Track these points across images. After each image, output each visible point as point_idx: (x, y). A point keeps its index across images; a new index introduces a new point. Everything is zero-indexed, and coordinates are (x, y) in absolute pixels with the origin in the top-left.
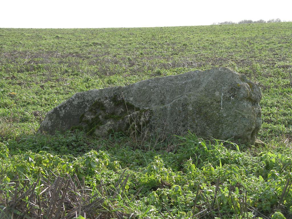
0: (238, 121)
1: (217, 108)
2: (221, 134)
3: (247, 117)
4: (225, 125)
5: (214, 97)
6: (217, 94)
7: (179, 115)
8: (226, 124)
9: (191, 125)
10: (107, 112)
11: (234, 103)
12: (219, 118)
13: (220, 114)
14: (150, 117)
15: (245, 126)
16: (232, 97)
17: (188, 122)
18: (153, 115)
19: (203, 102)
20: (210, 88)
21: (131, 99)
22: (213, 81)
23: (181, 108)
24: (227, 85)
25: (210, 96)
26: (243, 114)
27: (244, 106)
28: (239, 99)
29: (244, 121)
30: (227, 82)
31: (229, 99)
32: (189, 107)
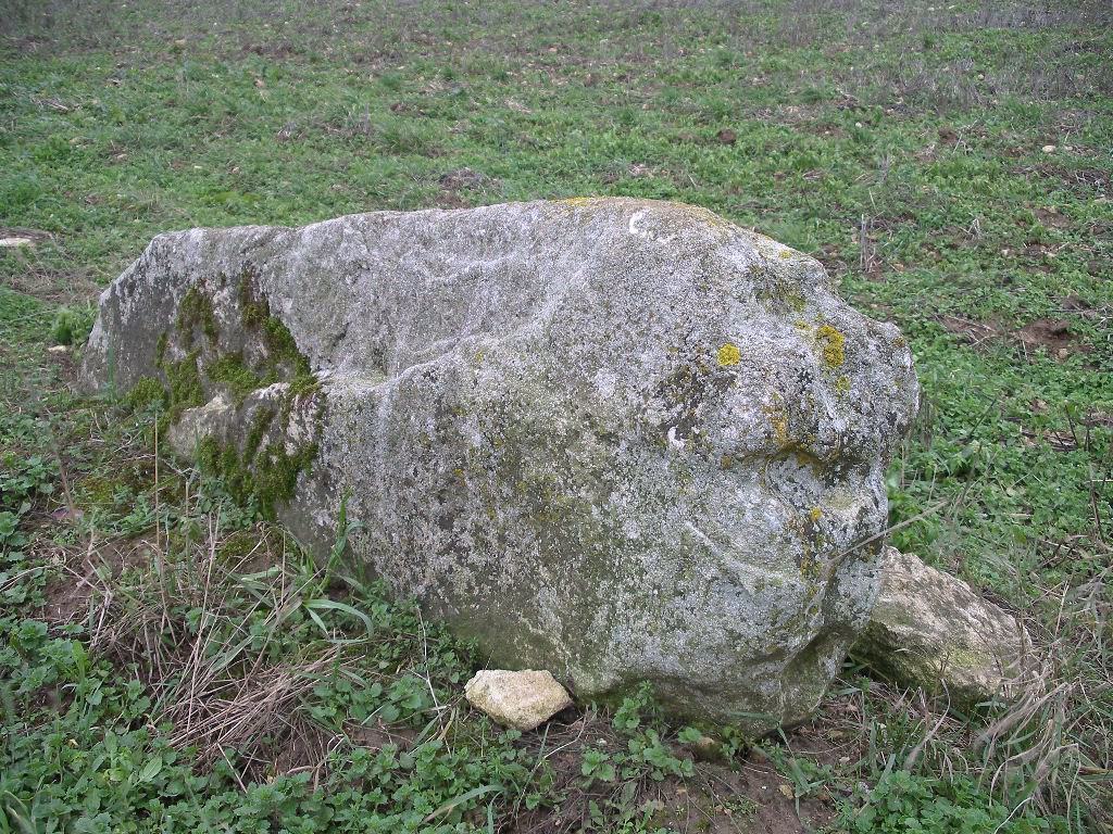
0: (692, 597)
1: (597, 474)
2: (604, 639)
3: (749, 587)
4: (625, 591)
5: (585, 399)
6: (605, 383)
7: (422, 459)
8: (632, 590)
9: (479, 529)
10: (222, 348)
11: (682, 475)
12: (600, 538)
13: (607, 514)
14: (319, 431)
15: (734, 637)
16: (672, 433)
17: (467, 506)
18: (327, 424)
19: (529, 417)
20: (572, 335)
21: (288, 306)
22: (592, 298)
23: (431, 422)
24: (657, 337)
25: (569, 388)
26: (728, 559)
27: (741, 511)
28: (711, 458)
29: (732, 606)
30: (660, 320)
31: (654, 440)
32: (465, 429)
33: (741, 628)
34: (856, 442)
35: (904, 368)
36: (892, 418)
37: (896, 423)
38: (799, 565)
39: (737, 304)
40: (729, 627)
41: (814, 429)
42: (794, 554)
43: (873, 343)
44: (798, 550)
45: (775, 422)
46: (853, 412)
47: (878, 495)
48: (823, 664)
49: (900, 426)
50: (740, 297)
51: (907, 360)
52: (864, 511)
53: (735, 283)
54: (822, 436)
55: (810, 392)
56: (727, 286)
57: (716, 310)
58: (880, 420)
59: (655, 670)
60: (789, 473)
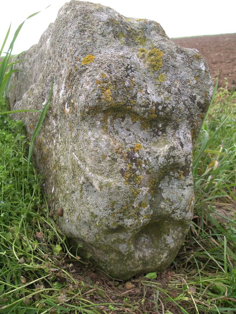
33: (96, 212)
34: (168, 109)
35: (200, 70)
36: (193, 98)
37: (196, 101)
38: (123, 175)
39: (101, 37)
40: (91, 211)
41: (135, 97)
42: (119, 168)
43: (179, 57)
44: (122, 166)
45: (103, 89)
46: (166, 93)
47: (183, 140)
48: (165, 239)
49: (199, 103)
50: (102, 34)
51: (202, 67)
52: (173, 148)
53: (99, 27)
54: (139, 101)
55: (133, 77)
56: (95, 28)
57: (88, 41)
58: (184, 98)
59: (70, 233)
60: (127, 126)
